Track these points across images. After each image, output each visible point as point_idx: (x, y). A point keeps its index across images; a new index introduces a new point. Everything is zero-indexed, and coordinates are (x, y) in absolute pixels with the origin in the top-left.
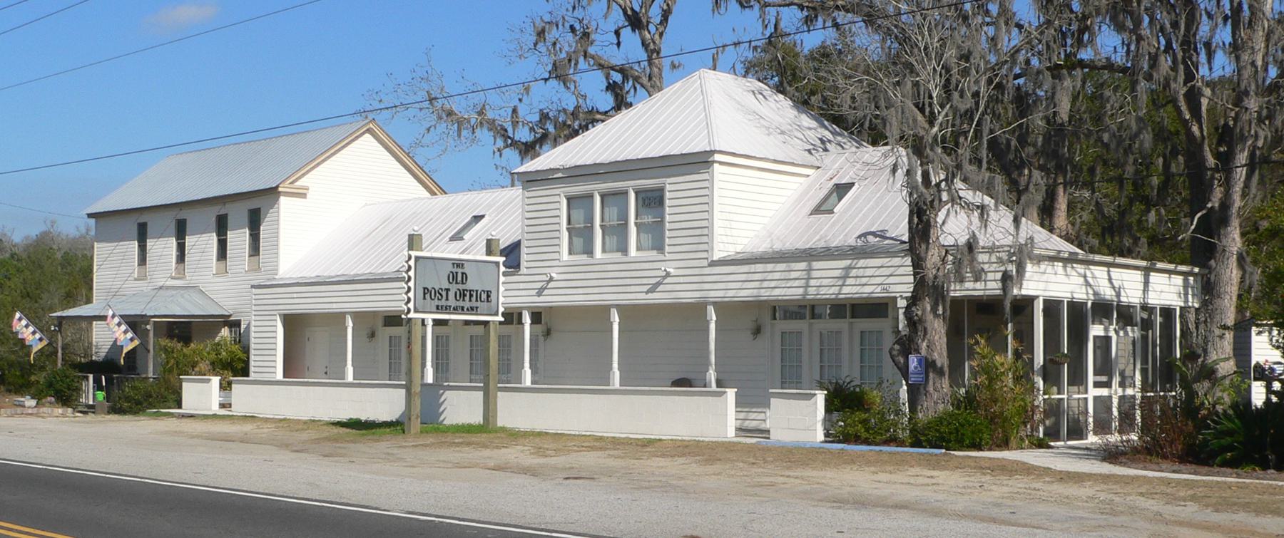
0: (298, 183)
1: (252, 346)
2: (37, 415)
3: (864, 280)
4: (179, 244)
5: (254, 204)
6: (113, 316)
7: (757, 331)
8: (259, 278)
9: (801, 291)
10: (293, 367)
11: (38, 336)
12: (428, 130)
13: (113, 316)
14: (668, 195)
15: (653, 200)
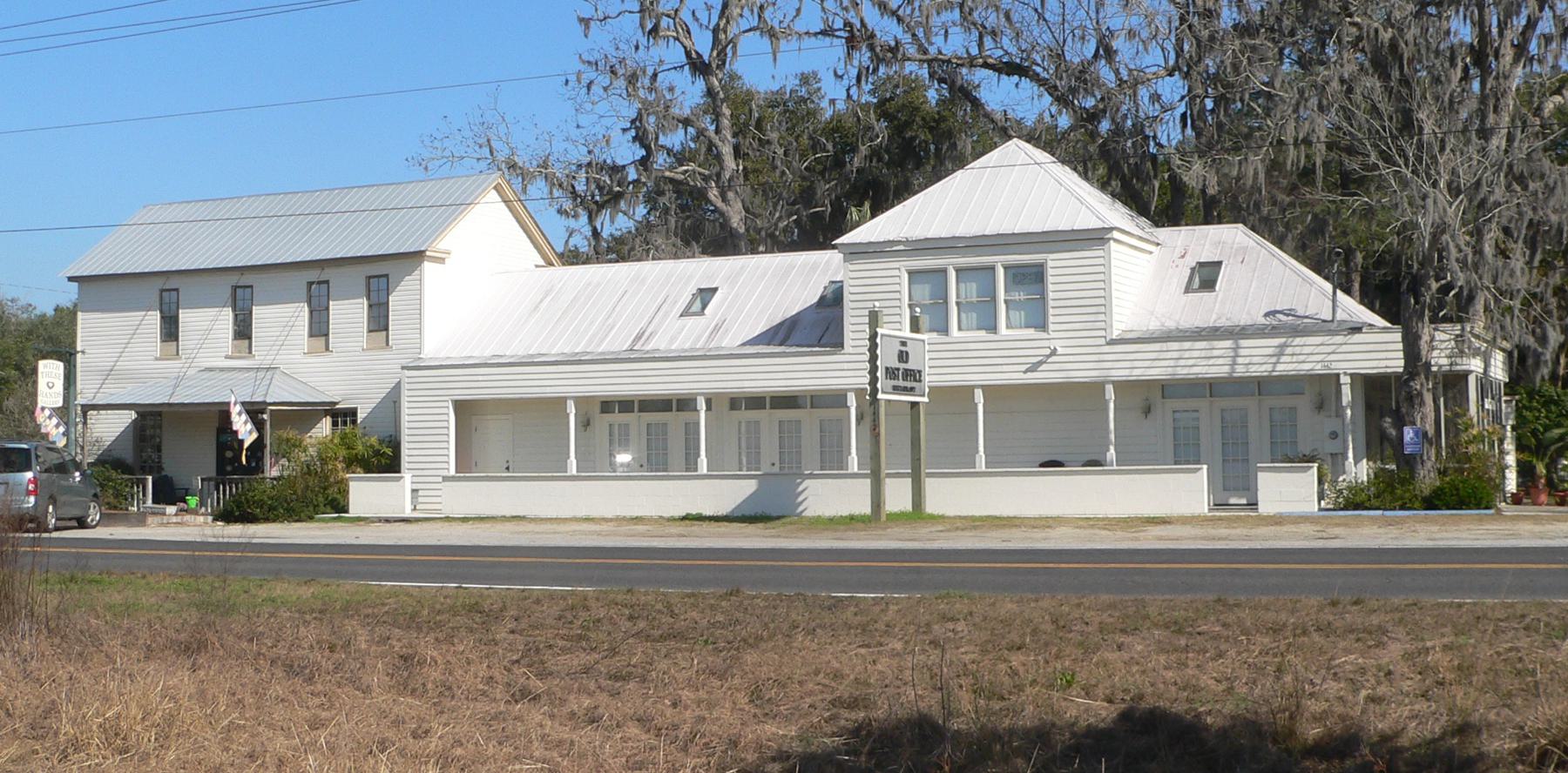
3: (1302, 358)
7: (1147, 411)
9: (1226, 369)
10: (467, 462)
14: (1050, 272)
15: (1031, 278)
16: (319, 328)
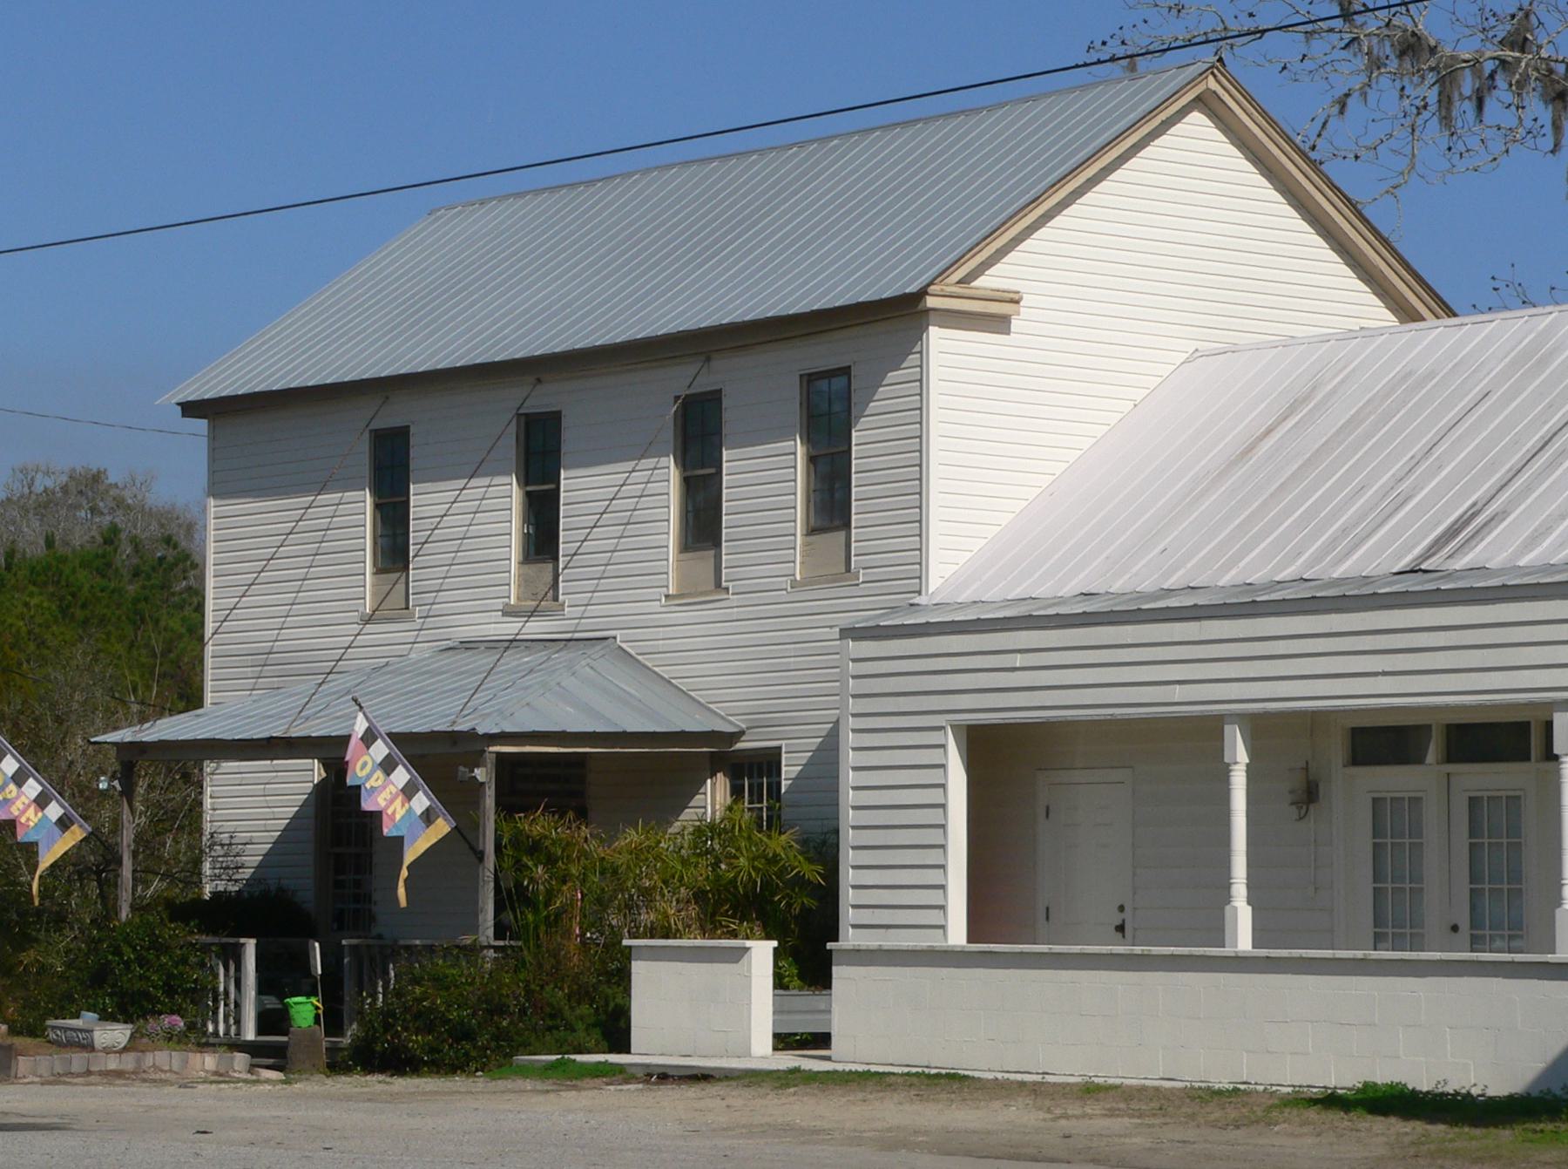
0: (984, 282)
1: (849, 837)
2: (136, 1075)
4: (691, 486)
5: (820, 354)
6: (369, 738)
8: (861, 606)
10: (1005, 903)
11: (54, 811)
12: (1342, 104)
13: (369, 738)
16: (702, 524)
